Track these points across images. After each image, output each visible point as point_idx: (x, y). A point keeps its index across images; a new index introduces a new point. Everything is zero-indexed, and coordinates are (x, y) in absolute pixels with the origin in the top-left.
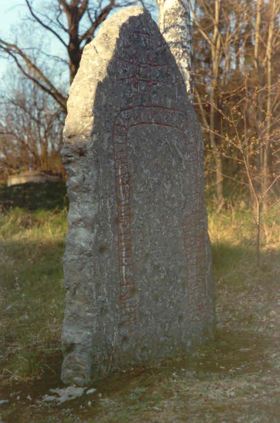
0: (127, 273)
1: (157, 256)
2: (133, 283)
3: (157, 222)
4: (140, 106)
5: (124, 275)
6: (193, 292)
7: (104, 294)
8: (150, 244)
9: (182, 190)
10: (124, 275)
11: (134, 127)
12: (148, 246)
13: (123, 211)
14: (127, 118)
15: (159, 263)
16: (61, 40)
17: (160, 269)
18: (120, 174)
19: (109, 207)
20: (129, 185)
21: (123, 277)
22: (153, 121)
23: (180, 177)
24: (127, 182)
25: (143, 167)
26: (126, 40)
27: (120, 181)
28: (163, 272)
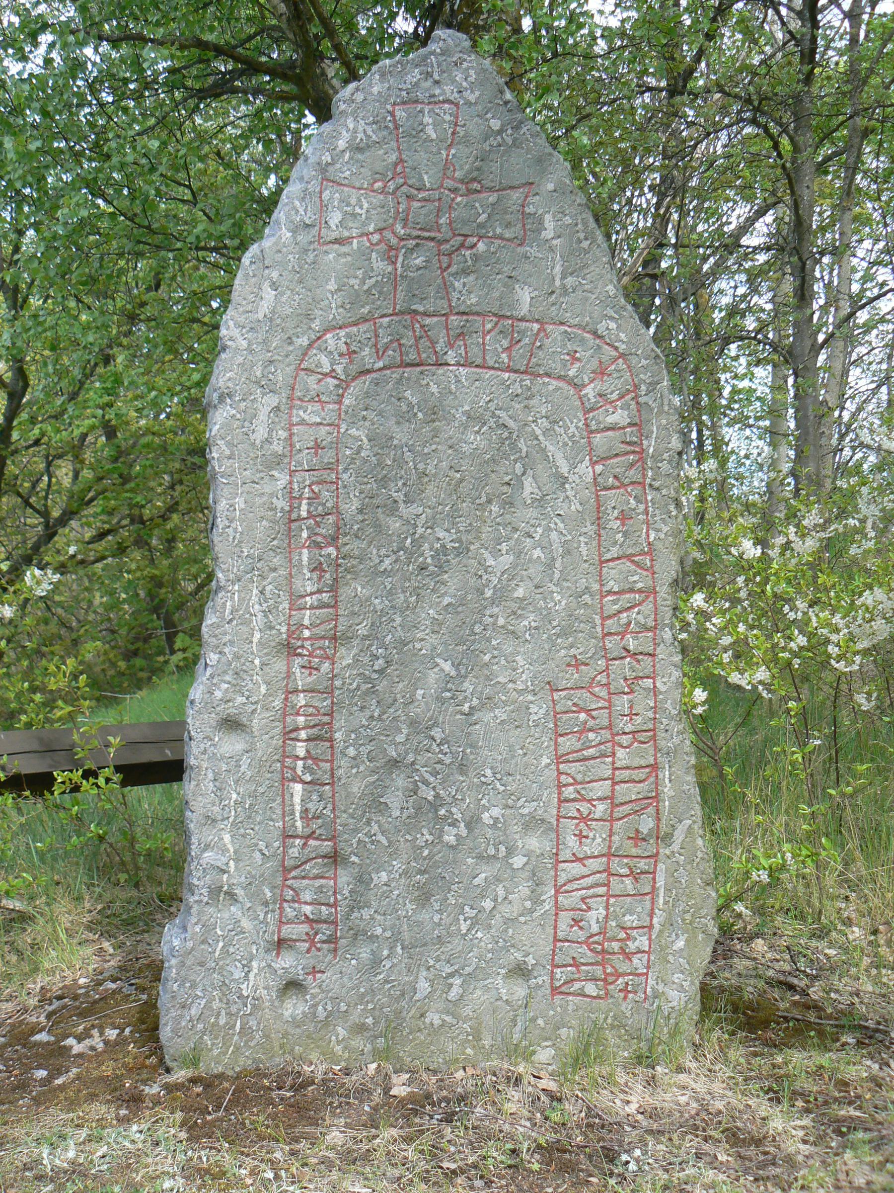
0: (310, 805)
1: (435, 774)
2: (333, 838)
3: (442, 670)
4: (402, 313)
5: (298, 808)
6: (667, 1155)
7: (225, 850)
8: (405, 731)
9: (557, 575)
10: (298, 808)
11: (369, 377)
12: (400, 738)
13: (306, 622)
14: (344, 349)
15: (437, 796)
16: (577, 761)
17: (442, 812)
18: (304, 514)
19: (257, 607)
20: (337, 548)
21: (293, 813)
22: (451, 357)
23: (554, 535)
24: (333, 540)
25: (400, 496)
26: (361, 129)
27: (305, 534)
28: (454, 824)
